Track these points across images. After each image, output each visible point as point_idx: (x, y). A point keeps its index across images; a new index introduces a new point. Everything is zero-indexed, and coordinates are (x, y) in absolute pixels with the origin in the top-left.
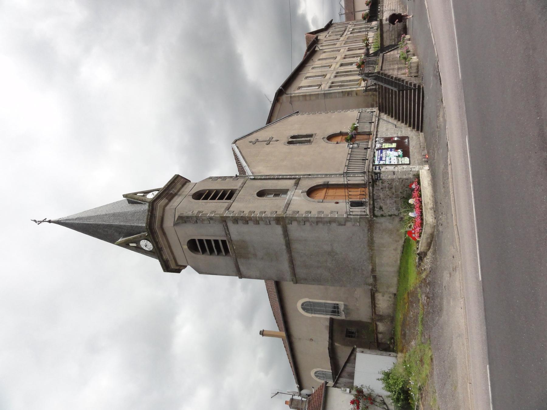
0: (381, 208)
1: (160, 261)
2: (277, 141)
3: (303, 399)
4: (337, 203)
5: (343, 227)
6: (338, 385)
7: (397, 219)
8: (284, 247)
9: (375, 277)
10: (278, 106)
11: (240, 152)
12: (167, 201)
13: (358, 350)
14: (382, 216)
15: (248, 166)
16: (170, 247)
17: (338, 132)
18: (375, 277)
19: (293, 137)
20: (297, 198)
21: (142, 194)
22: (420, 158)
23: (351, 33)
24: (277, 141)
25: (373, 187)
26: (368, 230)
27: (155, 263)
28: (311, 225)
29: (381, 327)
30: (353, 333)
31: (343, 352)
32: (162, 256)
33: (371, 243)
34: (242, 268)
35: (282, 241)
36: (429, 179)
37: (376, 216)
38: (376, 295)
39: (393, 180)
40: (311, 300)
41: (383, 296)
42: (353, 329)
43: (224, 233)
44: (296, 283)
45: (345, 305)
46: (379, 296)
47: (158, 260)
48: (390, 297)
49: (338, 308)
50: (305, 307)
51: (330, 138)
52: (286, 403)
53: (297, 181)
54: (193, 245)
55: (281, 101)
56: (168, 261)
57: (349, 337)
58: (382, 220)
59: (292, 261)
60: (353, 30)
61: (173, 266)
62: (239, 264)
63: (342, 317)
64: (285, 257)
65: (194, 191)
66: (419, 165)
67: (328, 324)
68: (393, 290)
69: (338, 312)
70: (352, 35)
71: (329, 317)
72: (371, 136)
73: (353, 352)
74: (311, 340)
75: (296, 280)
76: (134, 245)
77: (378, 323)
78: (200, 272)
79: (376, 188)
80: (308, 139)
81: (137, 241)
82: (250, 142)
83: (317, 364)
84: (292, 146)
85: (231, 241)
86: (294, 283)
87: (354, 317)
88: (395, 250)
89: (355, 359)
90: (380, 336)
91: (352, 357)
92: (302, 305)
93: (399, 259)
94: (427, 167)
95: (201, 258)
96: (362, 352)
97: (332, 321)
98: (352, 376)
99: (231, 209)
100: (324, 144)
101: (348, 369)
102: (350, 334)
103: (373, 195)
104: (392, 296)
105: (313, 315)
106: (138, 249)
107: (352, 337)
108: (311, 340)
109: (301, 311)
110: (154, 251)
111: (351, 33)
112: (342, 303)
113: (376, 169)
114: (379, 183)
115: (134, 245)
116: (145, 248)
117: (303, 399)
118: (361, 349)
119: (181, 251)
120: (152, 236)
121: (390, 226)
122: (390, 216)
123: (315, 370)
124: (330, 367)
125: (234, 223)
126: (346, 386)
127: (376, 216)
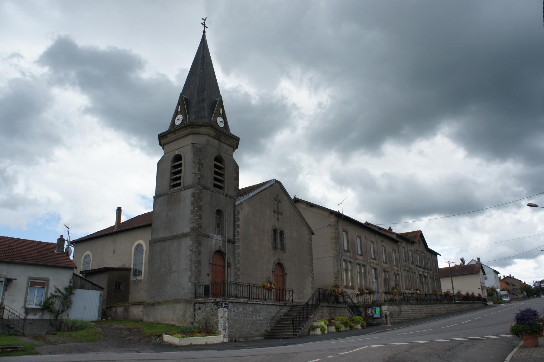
0: (200, 308)
1: (167, 131)
2: (278, 219)
3: (65, 249)
4: (208, 275)
5: (188, 280)
6: (75, 277)
7: (192, 321)
8: (175, 234)
9: (154, 304)
10: (327, 214)
11: (266, 188)
12: (213, 136)
13: (102, 292)
14: (195, 309)
15: (249, 198)
16: (177, 139)
17: (287, 271)
18: (154, 304)
19: (282, 233)
20: (214, 243)
21: (221, 112)
22: (236, 336)
23: (420, 275)
24: (278, 219)
25: (213, 302)
26: (186, 299)
27: (166, 128)
28: (190, 255)
29: (120, 310)
30: (119, 287)
31: (102, 280)
32: (170, 133)
33: (177, 301)
34: (161, 198)
35: (180, 232)
36: (215, 342)
37: (194, 305)
38: (142, 306)
39: (218, 317)
40: (144, 252)
41: (142, 311)
42: (122, 288)
43: (186, 185)
44: (150, 243)
45: (141, 280)
46: (141, 308)
47: (167, 129)
48: (140, 316)
49: (139, 275)
50: (139, 246)
51: (280, 265)
52: (62, 236)
53: (232, 242)
54: (178, 158)
55: (331, 216)
56: (167, 138)
57: (116, 284)
58: (192, 310)
59: (164, 240)
60: (425, 276)
61: (163, 141)
62: (164, 197)
63: (132, 279)
64: (168, 234)
65: (224, 156)
66: (229, 335)
67: (127, 266)
68: (145, 319)
69: (135, 275)
70: (417, 275)
71: (132, 267)
72: (264, 301)
73: (101, 288)
74: (114, 252)
75: (152, 243)
76: (179, 110)
77: (123, 307)
78: (158, 163)
79: (213, 304)
80: (279, 246)
81: (181, 113)
82: (277, 196)
83: (91, 259)
84: (271, 233)
85: (180, 190)
86: (150, 241)
87: (132, 288)
88: (172, 320)
89: (95, 290)
90: (114, 309)
91: (96, 287)
92: (141, 245)
93: (166, 323)
94: (226, 340)
95: (168, 165)
96: (101, 295)
97: (129, 270)
98: (82, 288)
99: (204, 191)
100: (274, 260)
101: (87, 285)
102: (118, 285)
103: (208, 303)
104: (141, 318)
105: (133, 254)
106: (177, 113)
107: (116, 287)
108: (114, 252)
109: (136, 243)
110: (175, 127)
111: (420, 275)
112: (143, 278)
113: (225, 304)
114: (216, 307)
115: (179, 110)
116: (177, 118)
117: (65, 249)
118: (102, 295)
119: (176, 147)
120: (184, 126)
121: (188, 316)
122: (195, 315)
123: (91, 255)
124: (94, 268)
125: (192, 193)
126: (75, 283)
127: (194, 305)
